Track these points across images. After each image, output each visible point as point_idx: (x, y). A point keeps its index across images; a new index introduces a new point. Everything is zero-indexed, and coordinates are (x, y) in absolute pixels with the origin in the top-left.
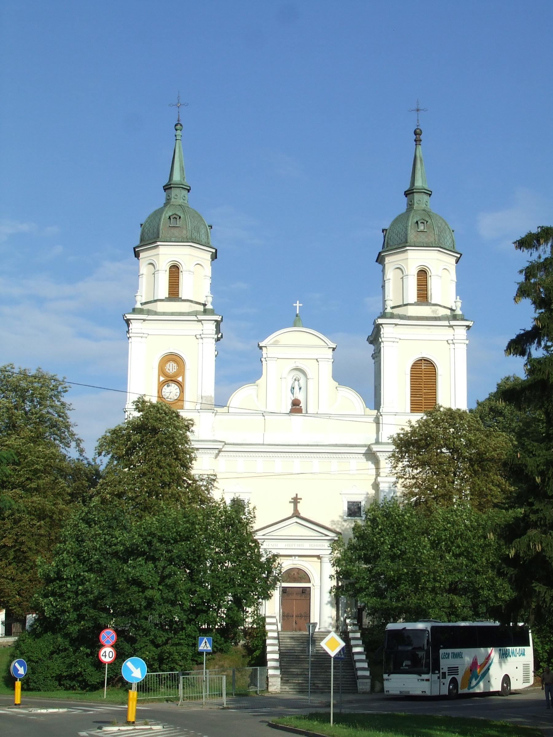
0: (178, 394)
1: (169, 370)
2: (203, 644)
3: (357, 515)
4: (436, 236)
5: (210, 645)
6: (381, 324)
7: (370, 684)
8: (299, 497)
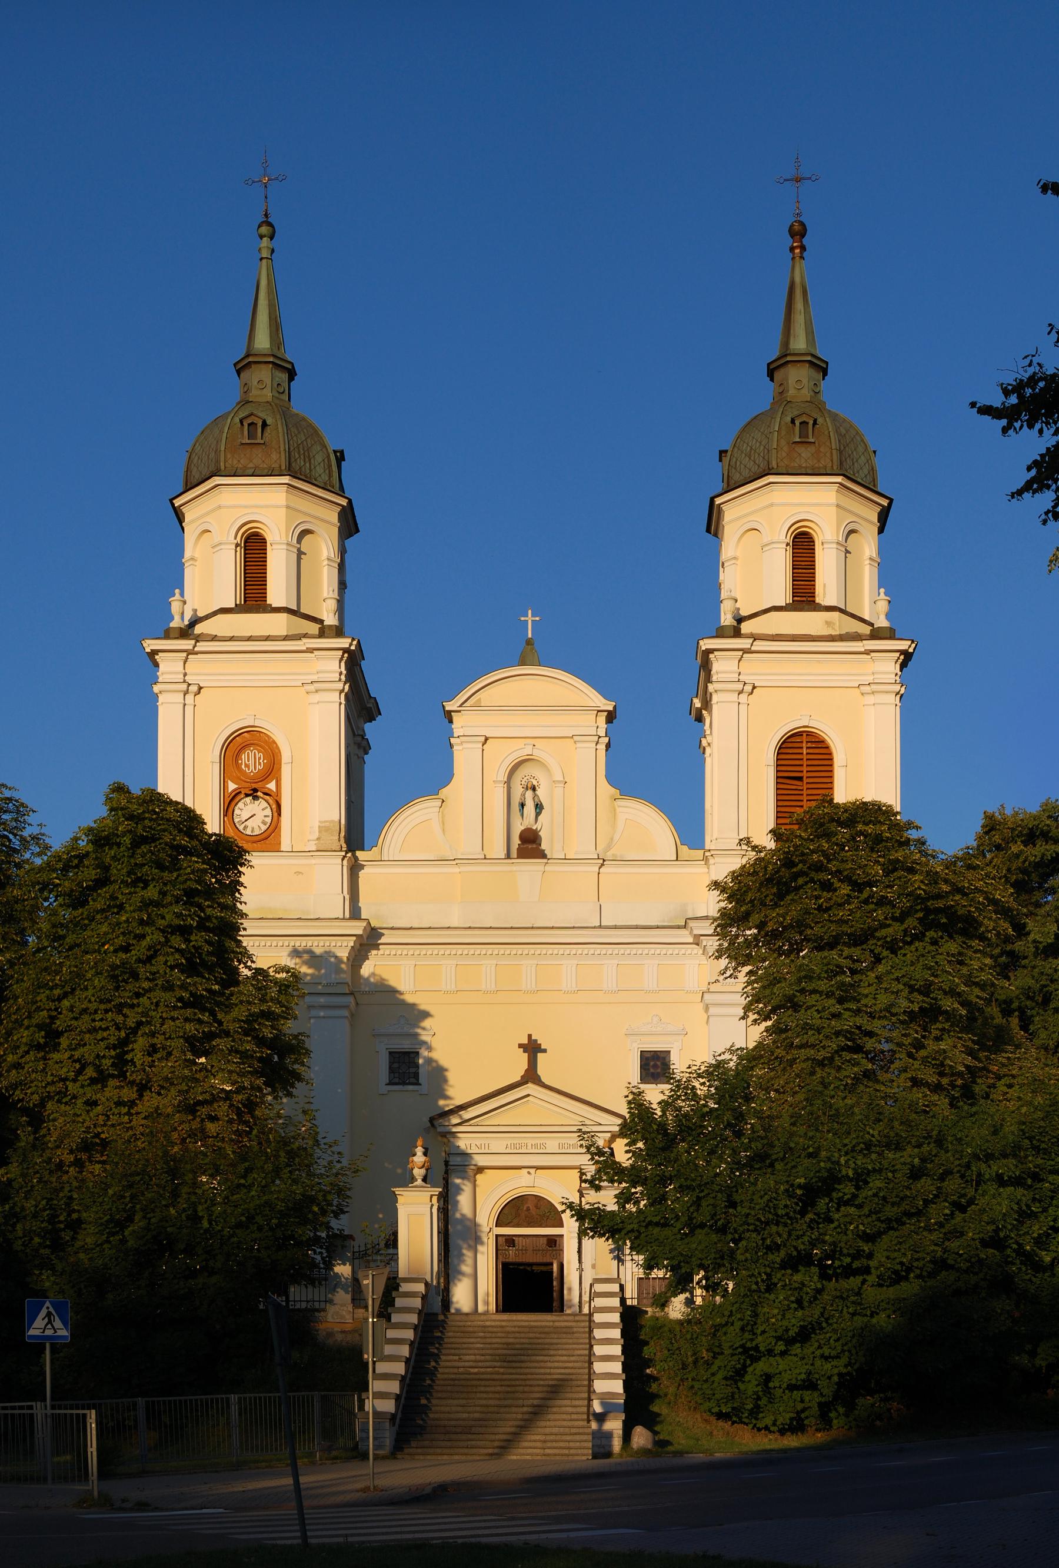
0: (268, 820)
1: (247, 766)
2: (40, 1322)
3: (648, 1055)
4: (834, 452)
5: (65, 1324)
6: (712, 651)
7: (621, 1432)
8: (526, 1041)
